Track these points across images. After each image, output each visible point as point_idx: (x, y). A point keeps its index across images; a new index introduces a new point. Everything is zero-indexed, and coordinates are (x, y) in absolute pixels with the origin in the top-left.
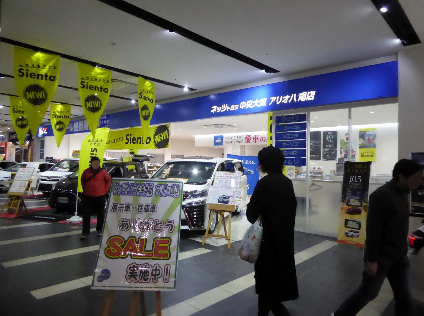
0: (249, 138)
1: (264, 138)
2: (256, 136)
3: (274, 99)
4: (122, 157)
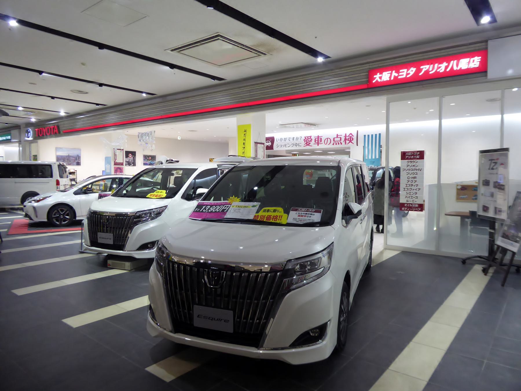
0: (309, 140)
1: (329, 140)
2: (318, 137)
3: (426, 68)
4: (346, 227)
